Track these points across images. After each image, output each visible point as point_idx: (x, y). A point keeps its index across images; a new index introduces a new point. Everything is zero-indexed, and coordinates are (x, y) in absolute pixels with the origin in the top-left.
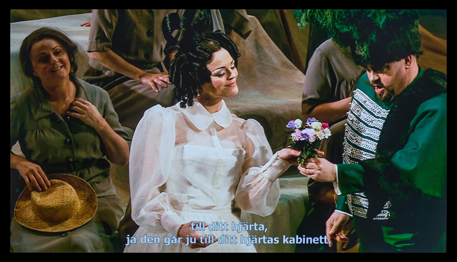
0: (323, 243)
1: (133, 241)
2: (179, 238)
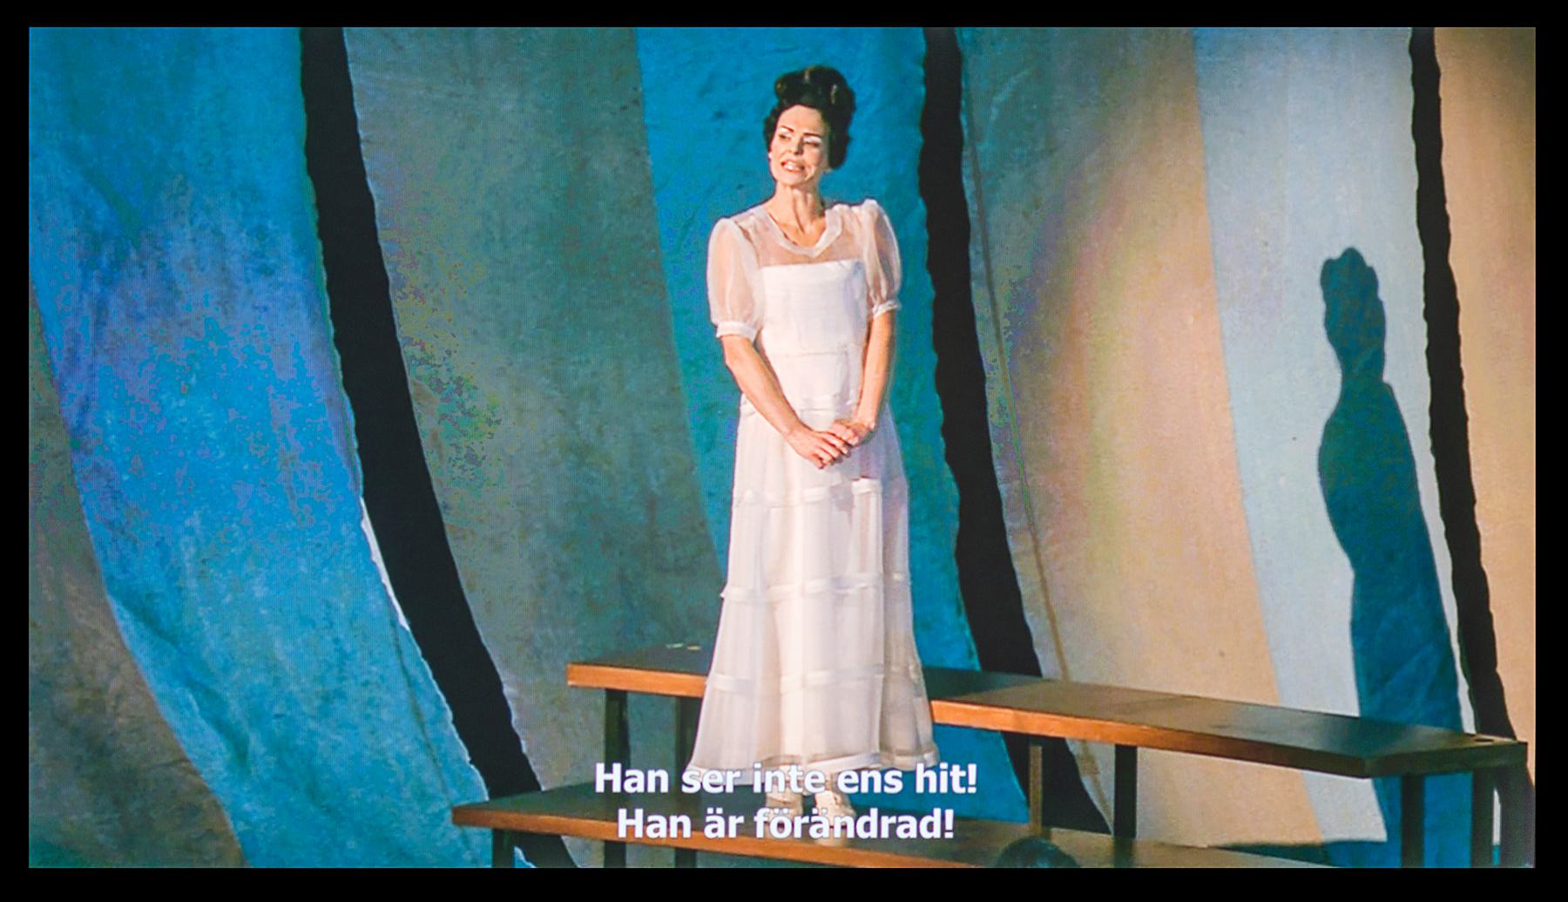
0: (963, 790)
1: (819, 831)
2: (733, 821)
